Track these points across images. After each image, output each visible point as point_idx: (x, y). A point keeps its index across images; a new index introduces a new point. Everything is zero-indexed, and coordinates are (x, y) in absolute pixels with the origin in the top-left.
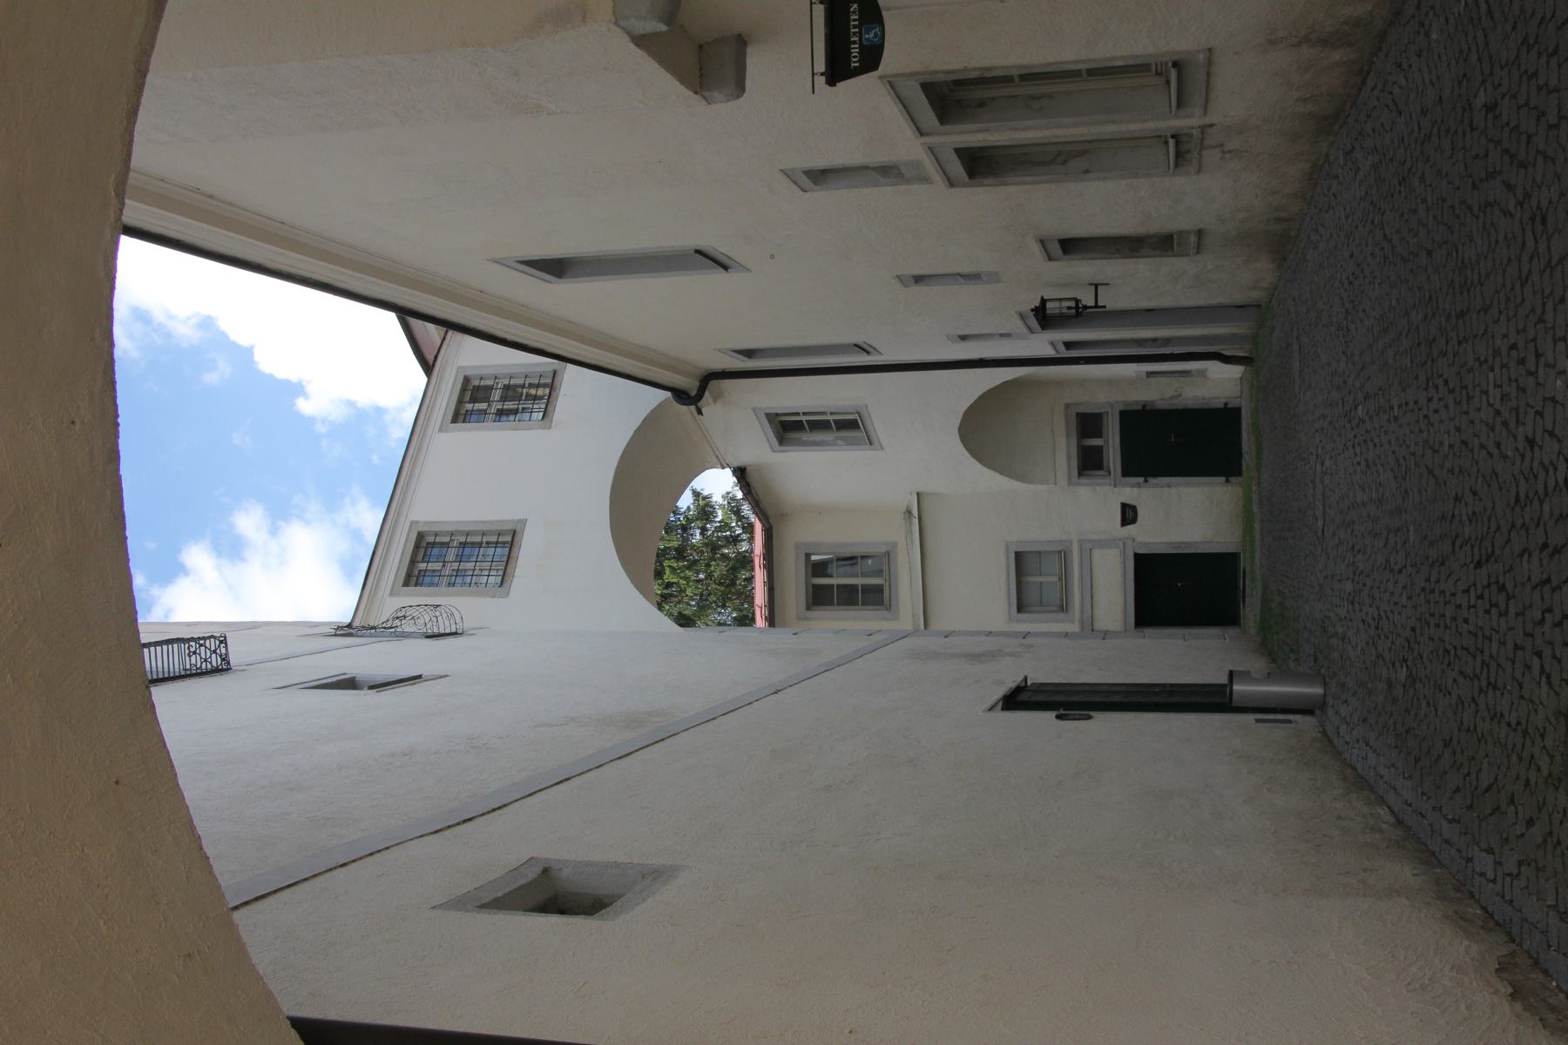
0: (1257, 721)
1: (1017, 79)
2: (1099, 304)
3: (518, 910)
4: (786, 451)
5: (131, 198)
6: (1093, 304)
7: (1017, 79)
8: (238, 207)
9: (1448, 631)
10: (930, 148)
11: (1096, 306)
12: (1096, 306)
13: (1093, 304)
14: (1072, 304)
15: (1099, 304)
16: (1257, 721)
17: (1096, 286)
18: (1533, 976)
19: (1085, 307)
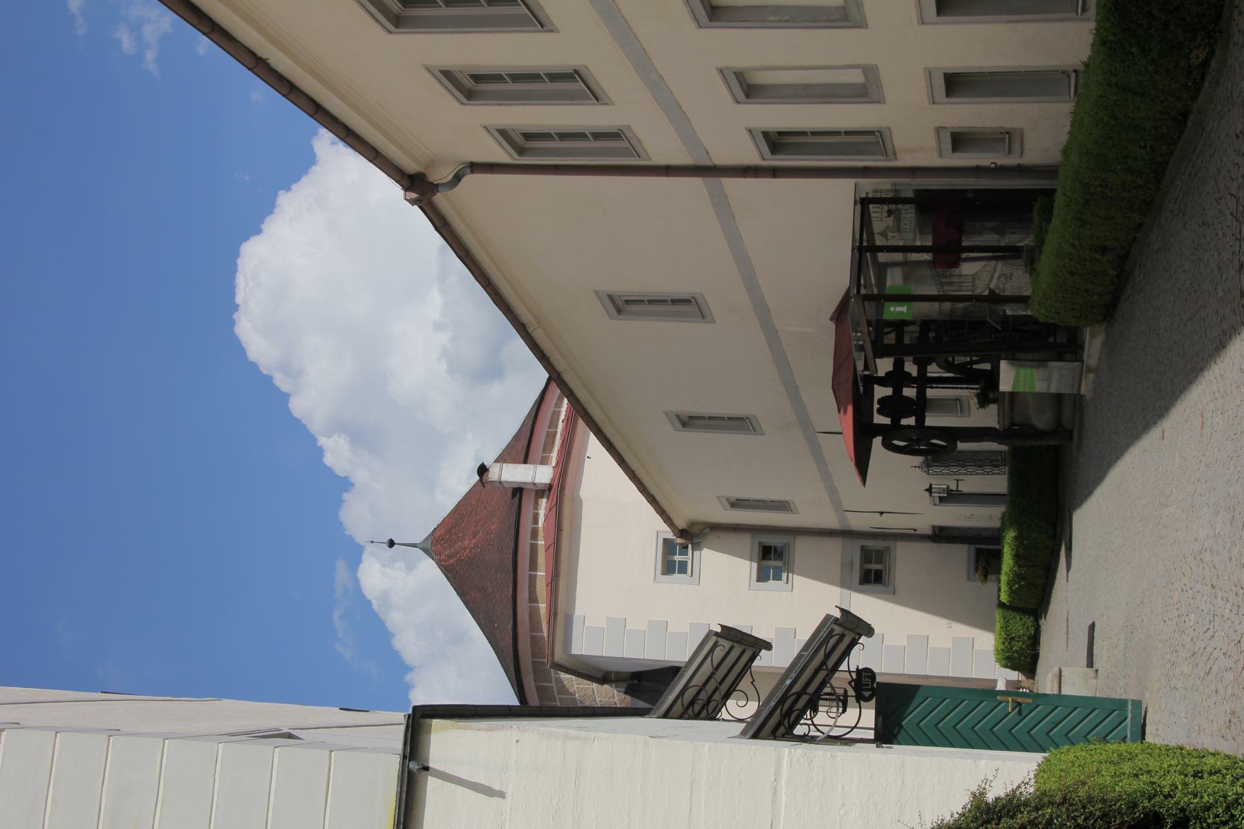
0: (782, 506)
1: (843, 133)
2: (959, 489)
3: (235, 276)
4: (378, 21)
5: (996, 687)
6: (955, 489)
7: (843, 133)
8: (889, 574)
9: (1228, 603)
10: (750, 131)
11: (957, 491)
12: (957, 491)
13: (955, 489)
14: (946, 487)
15: (959, 489)
16: (782, 506)
17: (958, 481)
18: (1016, 428)
19: (952, 491)
